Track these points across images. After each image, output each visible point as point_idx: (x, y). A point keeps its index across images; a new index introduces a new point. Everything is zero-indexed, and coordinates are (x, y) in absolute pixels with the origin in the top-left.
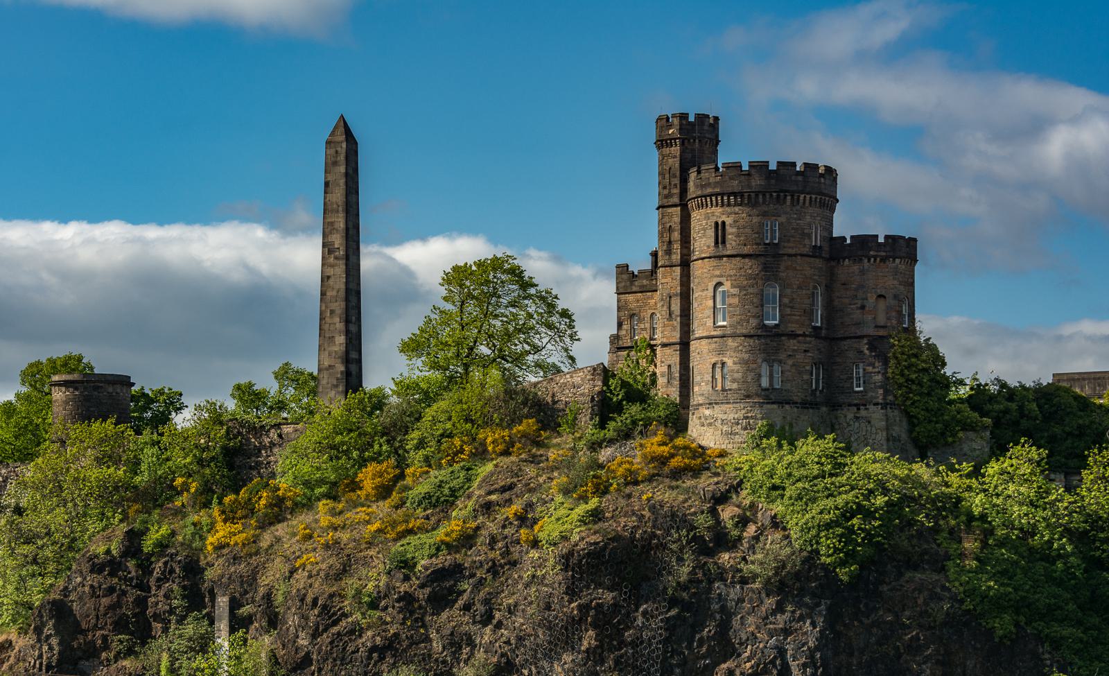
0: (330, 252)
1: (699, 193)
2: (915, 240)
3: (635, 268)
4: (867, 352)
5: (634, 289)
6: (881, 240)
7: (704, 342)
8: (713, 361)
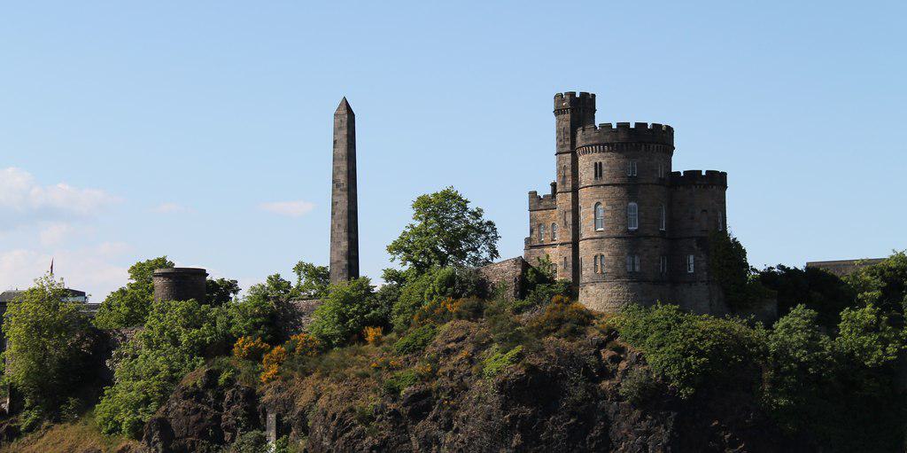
0: (338, 186)
1: (584, 144)
2: (725, 174)
3: (541, 194)
4: (696, 247)
5: (541, 207)
6: (704, 174)
7: (589, 241)
8: (595, 253)
